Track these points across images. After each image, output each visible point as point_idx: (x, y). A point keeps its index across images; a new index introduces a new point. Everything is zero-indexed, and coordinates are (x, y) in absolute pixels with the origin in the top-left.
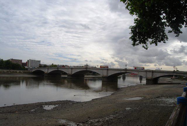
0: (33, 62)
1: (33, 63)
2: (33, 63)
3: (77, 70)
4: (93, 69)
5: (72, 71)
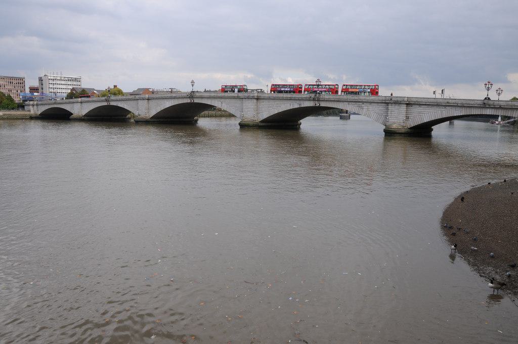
3: (162, 101)
4: (209, 98)
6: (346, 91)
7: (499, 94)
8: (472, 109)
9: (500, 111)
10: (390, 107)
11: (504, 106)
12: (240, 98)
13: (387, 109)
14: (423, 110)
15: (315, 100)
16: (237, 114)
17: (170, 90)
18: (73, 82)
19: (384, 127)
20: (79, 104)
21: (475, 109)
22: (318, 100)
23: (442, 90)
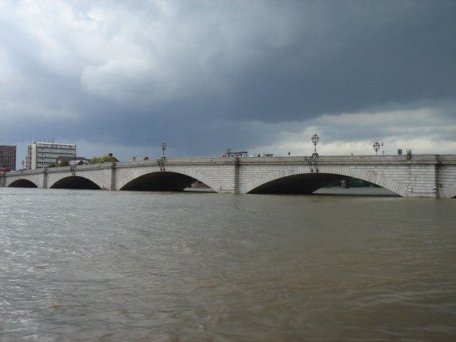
15: (311, 165)
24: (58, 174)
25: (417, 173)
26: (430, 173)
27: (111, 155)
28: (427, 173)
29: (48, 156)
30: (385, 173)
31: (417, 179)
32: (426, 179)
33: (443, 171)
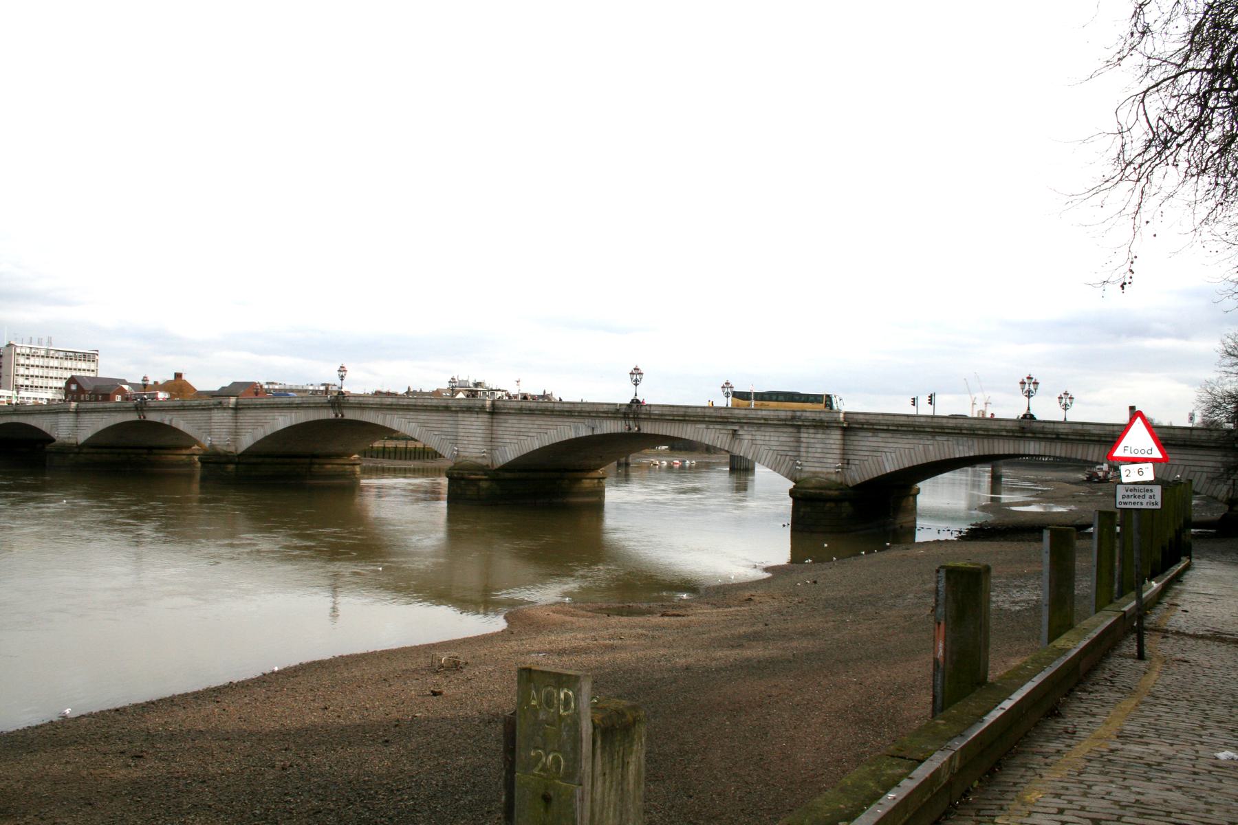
0: (32, 361)
1: (32, 371)
2: (32, 371)
3: (270, 415)
4: (382, 407)
5: (236, 433)
6: (27, 398)
7: (1066, 407)
8: (996, 442)
9: (1059, 445)
10: (805, 436)
11: (1067, 434)
12: (452, 411)
13: (798, 441)
14: (882, 444)
15: (629, 418)
16: (447, 450)
17: (322, 388)
18: (74, 362)
19: (791, 485)
20: (71, 417)
21: (1001, 441)
22: (634, 419)
23: (931, 397)
24: (106, 416)
25: (812, 441)
26: (832, 442)
27: (178, 376)
28: (828, 441)
29: (36, 372)
30: (758, 437)
31: (810, 450)
32: (825, 451)
33: (852, 438)
